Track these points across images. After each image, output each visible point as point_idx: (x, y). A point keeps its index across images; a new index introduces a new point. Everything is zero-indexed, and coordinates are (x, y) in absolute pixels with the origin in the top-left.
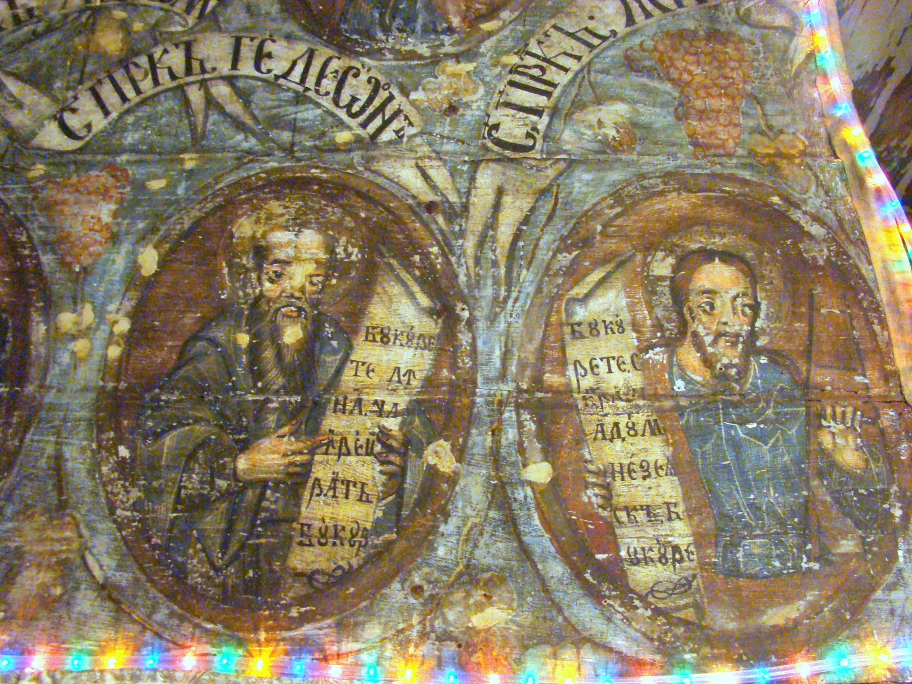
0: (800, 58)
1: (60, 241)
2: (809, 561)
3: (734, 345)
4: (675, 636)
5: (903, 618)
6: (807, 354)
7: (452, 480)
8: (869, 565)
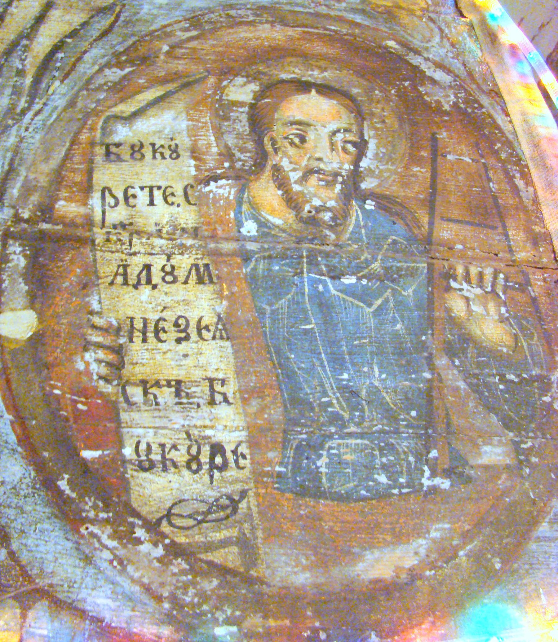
2: (433, 474)
4: (204, 597)
8: (527, 484)
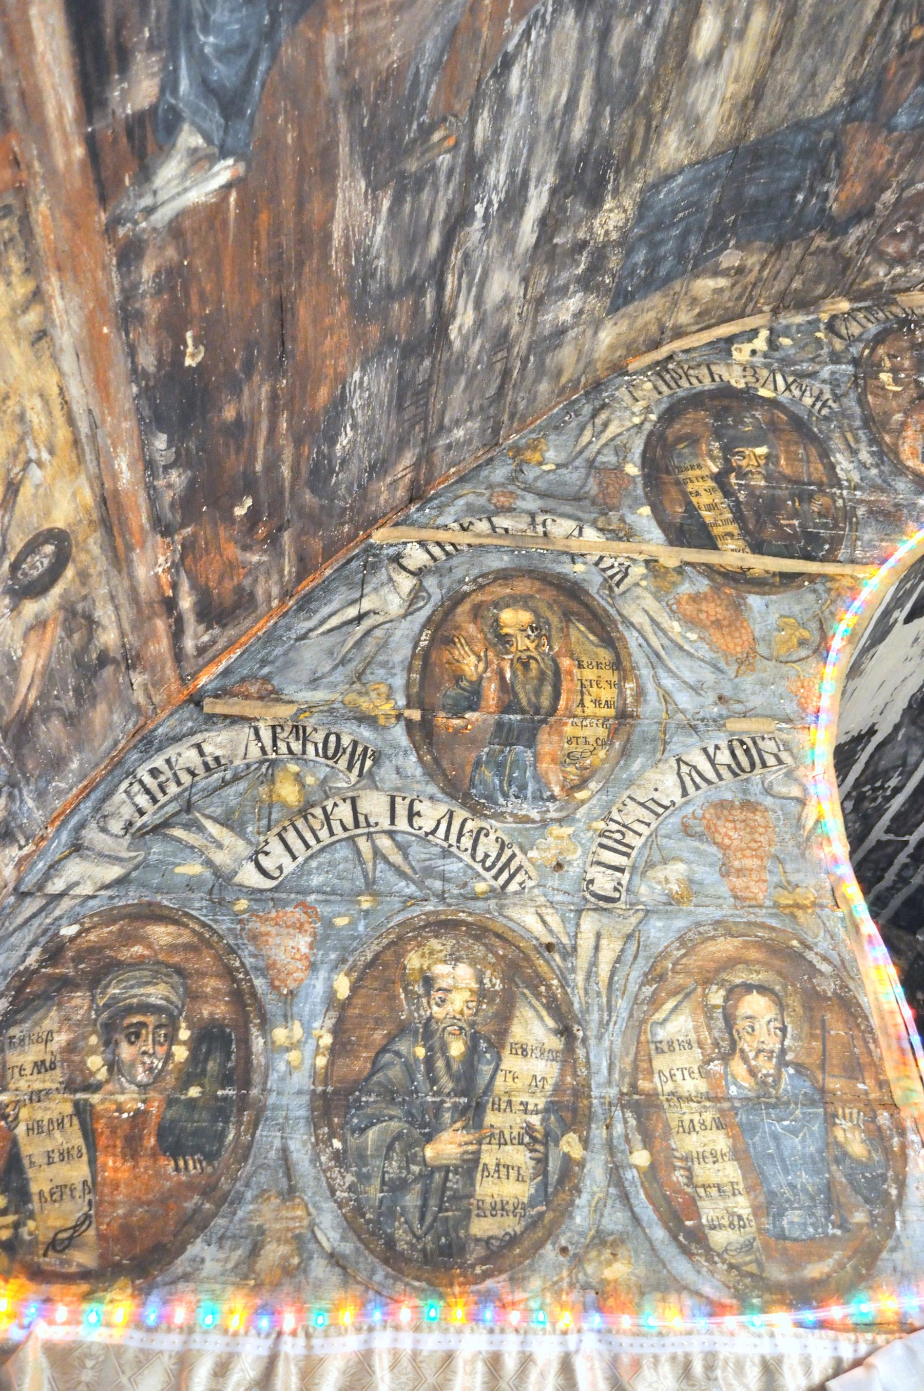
0: (810, 824)
1: (268, 968)
3: (770, 1058)
5: (903, 1274)
6: (822, 1067)
7: (582, 1164)
